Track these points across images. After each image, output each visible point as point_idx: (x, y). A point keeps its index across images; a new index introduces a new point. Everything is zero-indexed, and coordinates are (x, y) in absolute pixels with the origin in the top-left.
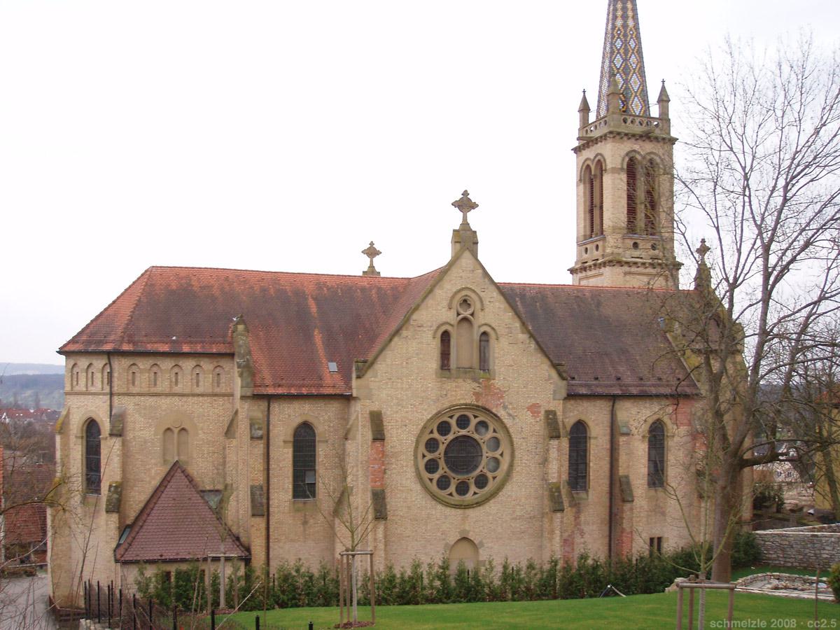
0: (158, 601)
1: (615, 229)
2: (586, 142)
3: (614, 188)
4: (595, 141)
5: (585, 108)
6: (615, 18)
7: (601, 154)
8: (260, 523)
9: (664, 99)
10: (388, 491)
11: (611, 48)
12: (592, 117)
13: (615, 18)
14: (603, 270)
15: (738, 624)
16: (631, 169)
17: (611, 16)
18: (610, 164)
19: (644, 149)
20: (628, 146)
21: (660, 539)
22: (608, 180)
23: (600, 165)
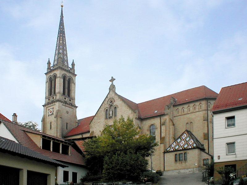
0: (93, 151)
1: (59, 93)
2: (50, 70)
3: (59, 83)
4: (54, 70)
5: (49, 63)
6: (60, 40)
7: (56, 74)
8: (206, 141)
9: (73, 65)
10: (174, 162)
11: (59, 48)
12: (51, 66)
13: (60, 40)
14: (55, 103)
15: (75, 175)
16: (64, 78)
17: (57, 48)
18: (58, 76)
19: (68, 74)
20: (64, 72)
21: (176, 161)
22: (58, 80)
23: (55, 77)
